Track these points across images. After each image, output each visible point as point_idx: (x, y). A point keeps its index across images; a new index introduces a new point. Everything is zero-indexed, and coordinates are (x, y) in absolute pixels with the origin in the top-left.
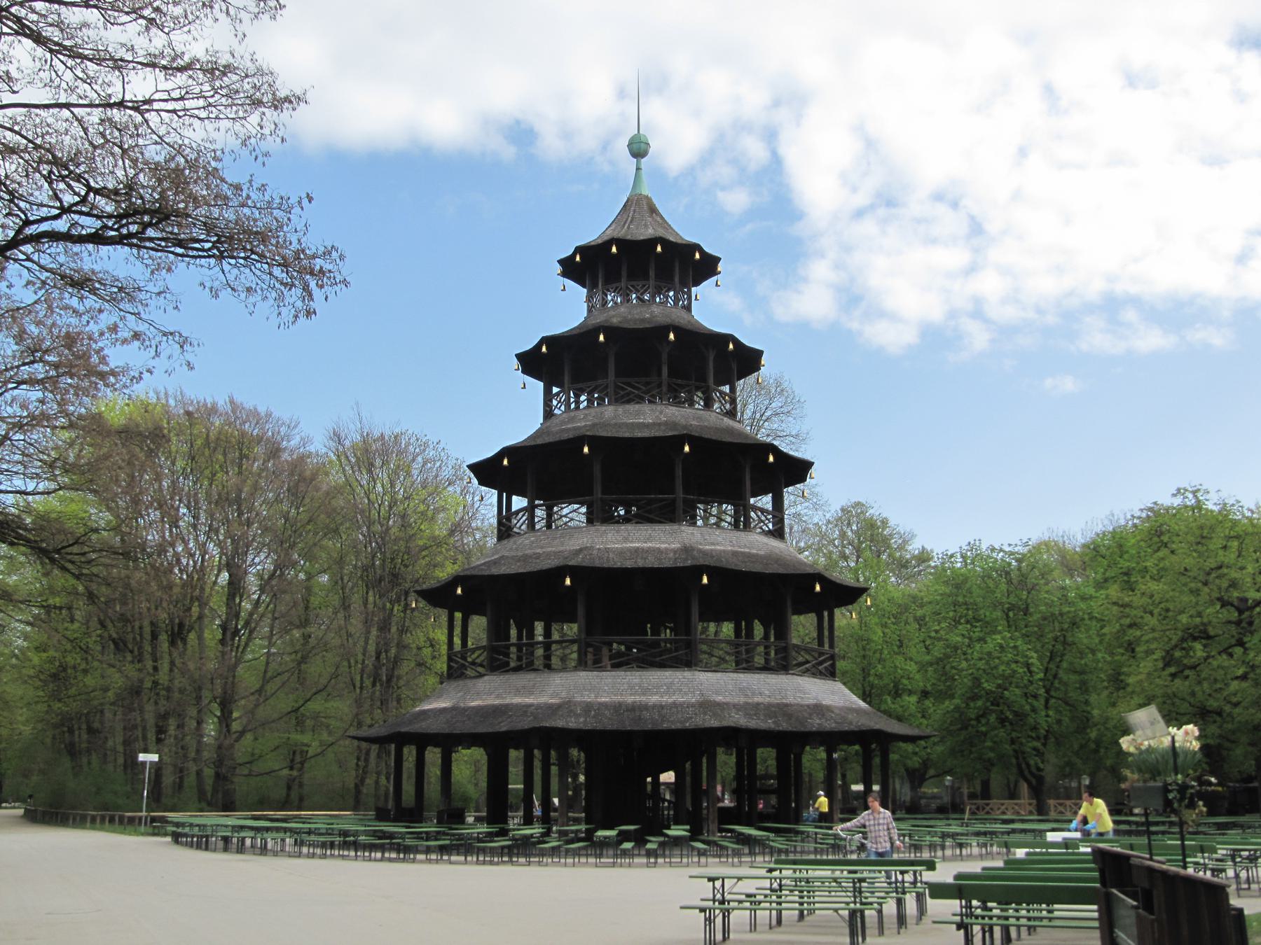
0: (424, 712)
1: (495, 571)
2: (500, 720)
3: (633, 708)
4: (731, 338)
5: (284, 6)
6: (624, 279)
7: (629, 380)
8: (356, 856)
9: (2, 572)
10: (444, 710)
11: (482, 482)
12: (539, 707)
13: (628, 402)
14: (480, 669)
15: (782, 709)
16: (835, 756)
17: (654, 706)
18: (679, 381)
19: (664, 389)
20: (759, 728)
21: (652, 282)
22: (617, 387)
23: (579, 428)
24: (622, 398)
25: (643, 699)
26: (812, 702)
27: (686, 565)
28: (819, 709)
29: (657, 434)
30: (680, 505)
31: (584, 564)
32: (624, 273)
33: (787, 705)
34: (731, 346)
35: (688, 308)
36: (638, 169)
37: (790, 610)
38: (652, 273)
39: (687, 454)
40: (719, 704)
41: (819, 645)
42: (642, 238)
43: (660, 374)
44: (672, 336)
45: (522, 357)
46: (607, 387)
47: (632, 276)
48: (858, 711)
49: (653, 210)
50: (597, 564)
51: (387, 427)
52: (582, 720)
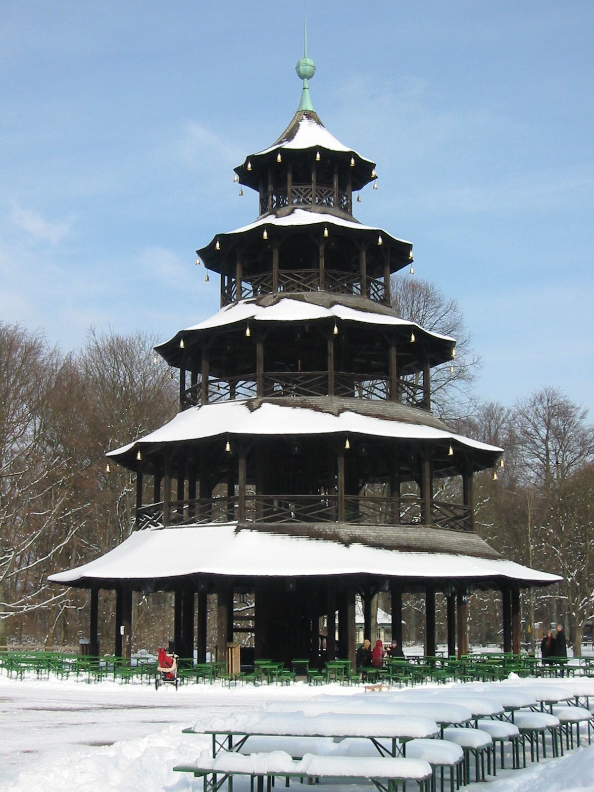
5: (360, 202)
7: (288, 271)
18: (335, 271)
19: (321, 278)
21: (313, 186)
30: (331, 382)
34: (380, 240)
38: (313, 178)
48: (483, 547)
51: (134, 335)
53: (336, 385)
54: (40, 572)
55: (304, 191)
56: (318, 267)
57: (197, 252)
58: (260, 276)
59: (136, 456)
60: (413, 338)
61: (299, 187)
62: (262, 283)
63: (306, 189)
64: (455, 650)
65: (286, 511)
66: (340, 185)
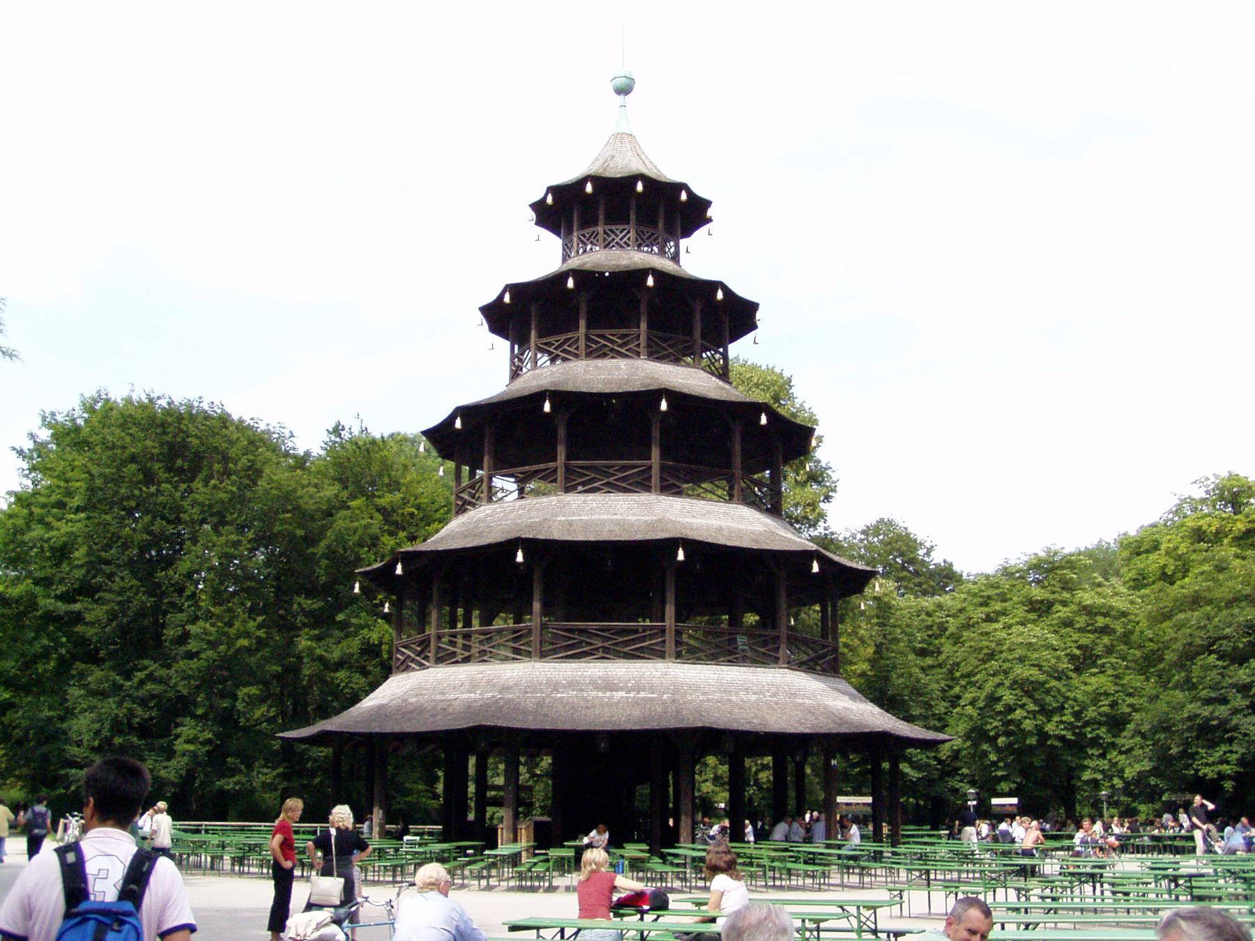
6: (601, 222)
13: (604, 355)
14: (1208, 595)
16: (834, 762)
22: (588, 338)
30: (655, 472)
32: (601, 217)
38: (633, 217)
41: (823, 637)
47: (610, 220)
53: (662, 479)
54: (1165, 686)
55: (621, 232)
56: (639, 327)
57: (711, 202)
58: (562, 338)
59: (395, 569)
61: (613, 228)
62: (565, 347)
65: (523, 645)
66: (665, 224)
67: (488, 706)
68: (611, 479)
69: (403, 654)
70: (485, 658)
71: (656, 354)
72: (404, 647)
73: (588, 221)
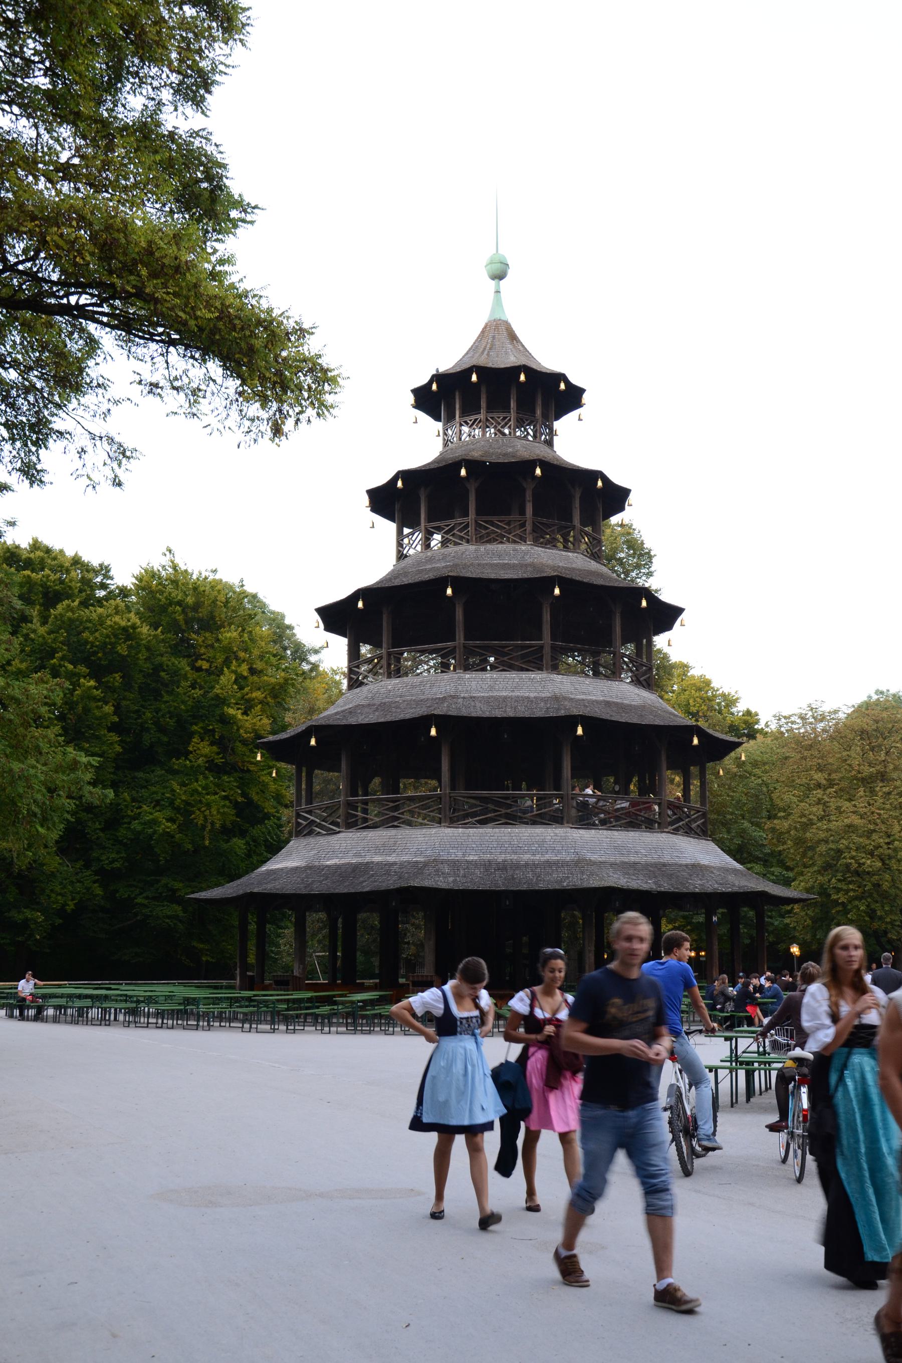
0: (274, 872)
1: (353, 721)
2: (361, 879)
3: (503, 867)
4: (599, 474)
7: (490, 518)
8: (251, 1027)
9: (2, 668)
10: (296, 869)
11: (329, 628)
12: (402, 865)
15: (659, 869)
17: (527, 865)
20: (641, 888)
21: (513, 414)
22: (478, 525)
23: (438, 569)
24: (484, 538)
25: (515, 857)
26: (689, 861)
27: (559, 714)
28: (696, 869)
29: (525, 576)
30: (547, 651)
31: (450, 713)
32: (483, 404)
33: (664, 865)
35: (550, 443)
36: (498, 292)
37: (664, 765)
38: (513, 404)
39: (557, 597)
40: (592, 863)
42: (502, 366)
43: (522, 512)
44: (538, 471)
45: (372, 493)
46: (467, 526)
48: (735, 871)
49: (513, 337)
50: (464, 712)
52: (451, 879)
60: (696, 741)
61: (495, 415)
63: (504, 418)
64: (55, 304)
67: (419, 868)
68: (505, 659)
69: (306, 819)
70: (395, 824)
71: (540, 537)
72: (307, 812)
73: (470, 408)
